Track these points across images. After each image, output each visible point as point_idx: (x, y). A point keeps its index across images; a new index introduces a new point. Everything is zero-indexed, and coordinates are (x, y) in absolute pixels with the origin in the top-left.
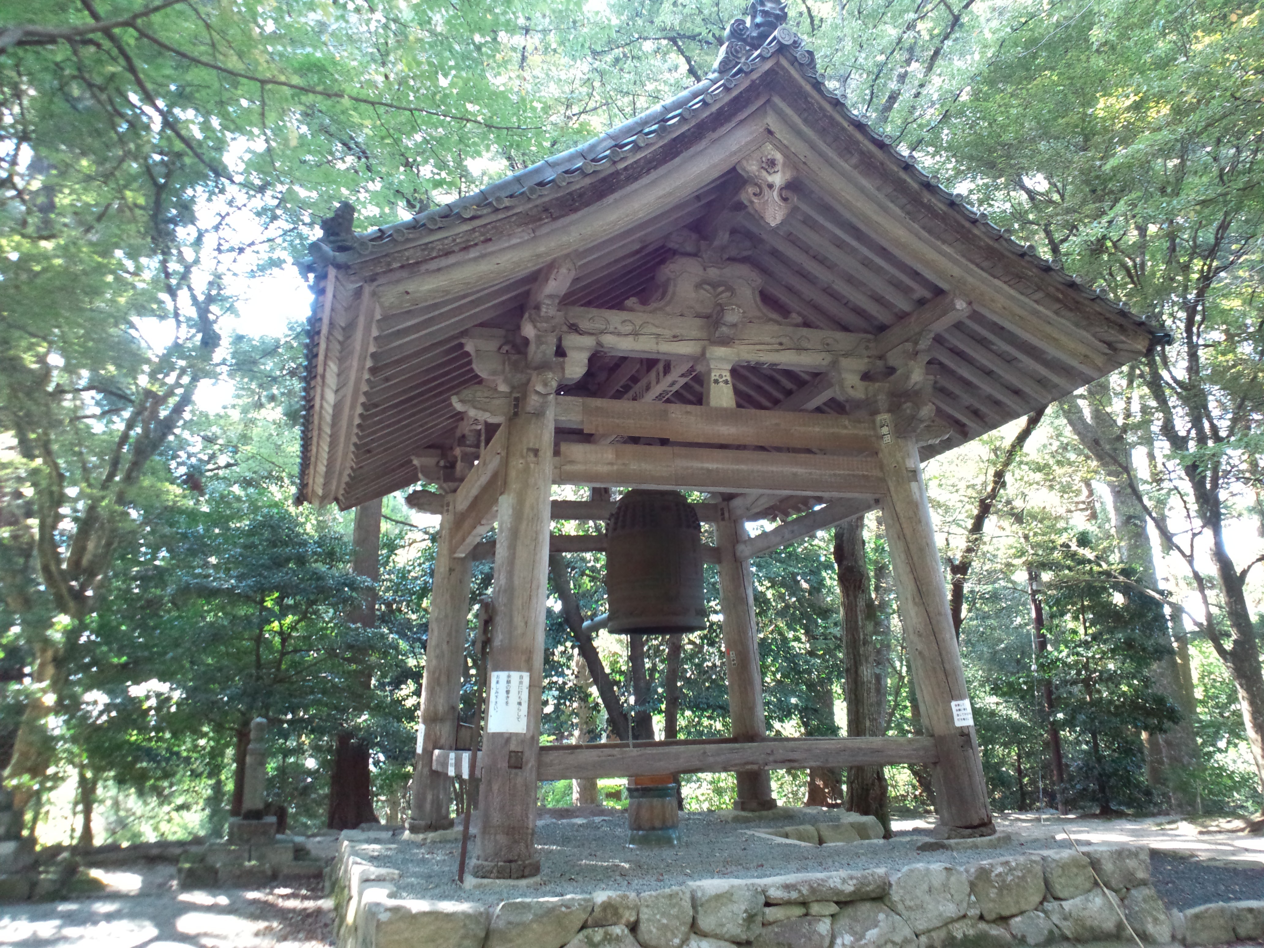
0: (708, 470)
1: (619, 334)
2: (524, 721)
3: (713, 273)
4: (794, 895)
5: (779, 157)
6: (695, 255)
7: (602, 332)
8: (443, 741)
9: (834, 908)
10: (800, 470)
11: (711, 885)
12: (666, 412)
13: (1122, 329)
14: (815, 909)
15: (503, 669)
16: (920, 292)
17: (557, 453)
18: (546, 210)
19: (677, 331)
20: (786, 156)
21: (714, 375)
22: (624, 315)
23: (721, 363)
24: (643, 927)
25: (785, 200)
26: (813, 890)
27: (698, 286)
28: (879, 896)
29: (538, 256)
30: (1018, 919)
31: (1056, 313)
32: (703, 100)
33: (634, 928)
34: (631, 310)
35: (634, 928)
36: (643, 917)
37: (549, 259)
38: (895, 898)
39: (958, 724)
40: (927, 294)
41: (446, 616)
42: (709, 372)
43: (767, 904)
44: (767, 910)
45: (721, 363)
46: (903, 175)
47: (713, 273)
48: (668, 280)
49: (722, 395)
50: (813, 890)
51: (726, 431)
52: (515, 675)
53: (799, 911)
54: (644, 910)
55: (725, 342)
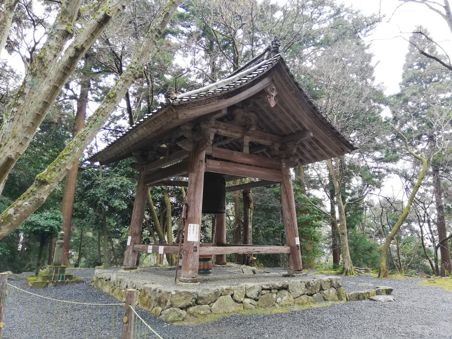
0: (242, 171)
1: (222, 129)
2: (198, 238)
3: (246, 114)
4: (269, 287)
5: (275, 88)
6: (241, 108)
7: (218, 128)
8: (137, 242)
9: (276, 291)
10: (264, 173)
11: (250, 285)
12: (233, 153)
13: (347, 146)
14: (273, 291)
15: (192, 223)
16: (299, 128)
17: (206, 162)
18: (224, 96)
19: (237, 130)
20: (276, 88)
21: (245, 144)
22: (224, 124)
23: (247, 140)
24: (235, 295)
25: (275, 100)
26: (273, 286)
27: (242, 118)
28: (285, 288)
29: (217, 108)
30: (315, 295)
31: (332, 140)
32: (263, 70)
33: (232, 295)
34: (226, 122)
35: (232, 295)
36: (235, 293)
37: (220, 109)
38: (290, 289)
39: (297, 244)
40: (301, 130)
41: (141, 203)
42: (243, 143)
43: (262, 290)
44: (262, 291)
45: (247, 140)
46: (304, 98)
47: (246, 114)
48: (235, 115)
49: (246, 150)
50: (273, 286)
51: (247, 160)
52: (195, 225)
53: (269, 291)
54: (235, 291)
55: (249, 135)
